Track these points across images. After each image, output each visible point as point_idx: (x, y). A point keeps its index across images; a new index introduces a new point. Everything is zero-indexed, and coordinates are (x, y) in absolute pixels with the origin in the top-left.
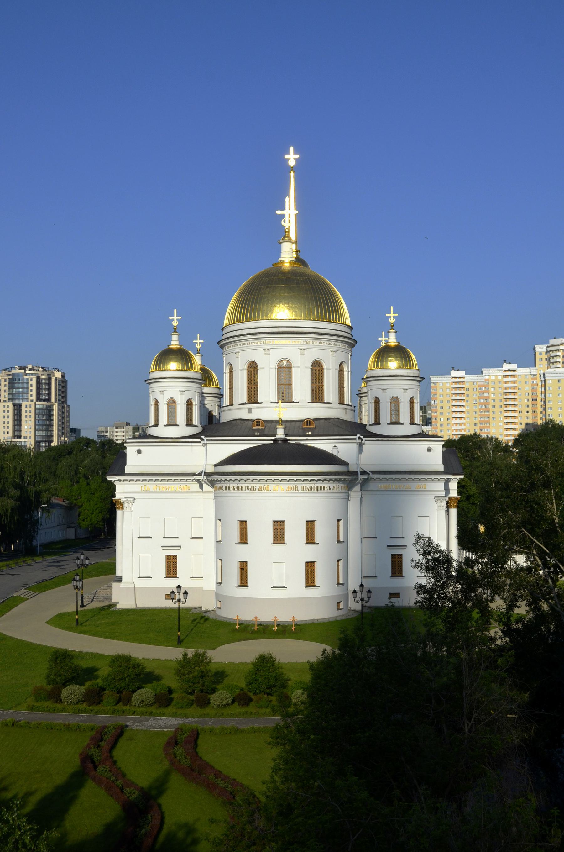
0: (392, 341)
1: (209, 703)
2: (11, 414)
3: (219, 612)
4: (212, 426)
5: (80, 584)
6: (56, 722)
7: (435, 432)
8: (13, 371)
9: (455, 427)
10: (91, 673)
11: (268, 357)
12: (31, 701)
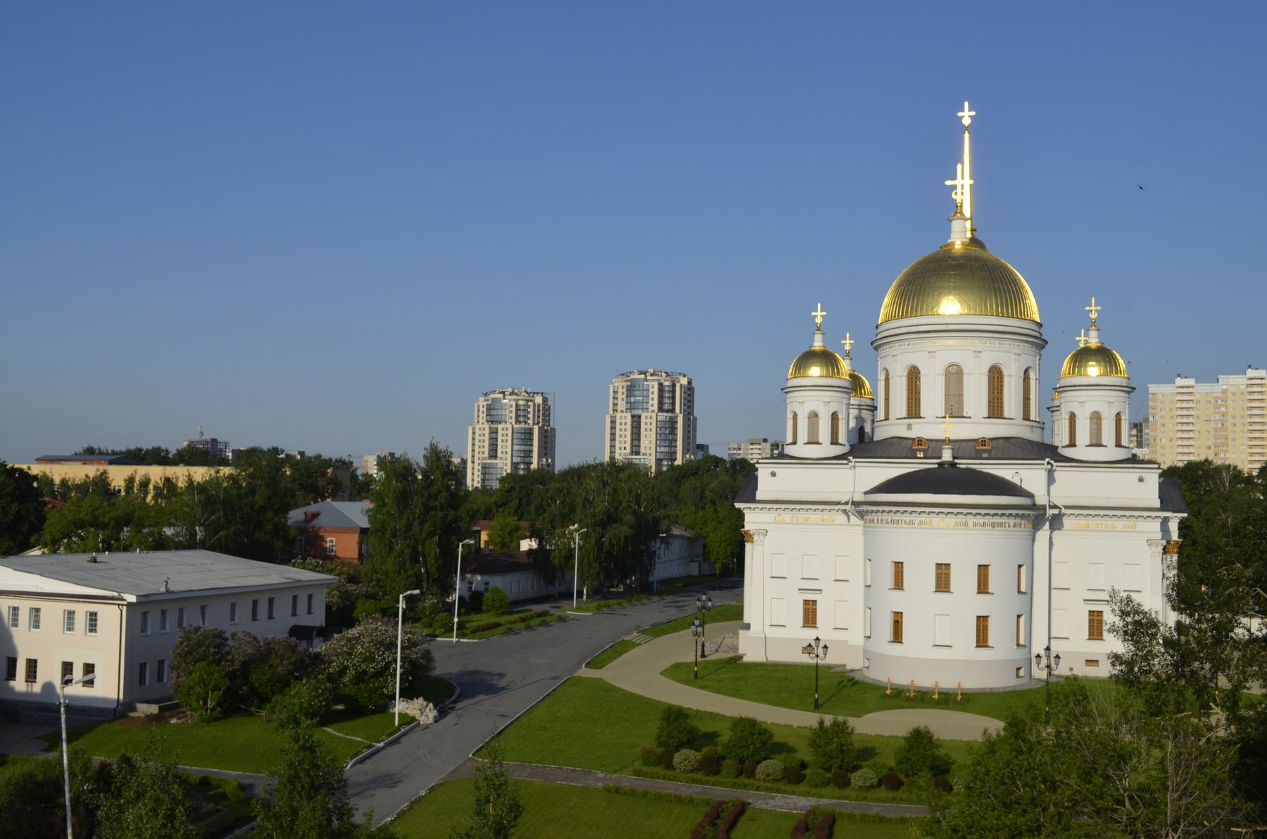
0: (1094, 342)
1: (849, 783)
2: (629, 427)
3: (866, 672)
4: (863, 445)
5: (700, 629)
6: (666, 792)
7: (1152, 457)
8: (632, 377)
9: (1180, 450)
10: (712, 737)
11: (933, 361)
12: (638, 765)
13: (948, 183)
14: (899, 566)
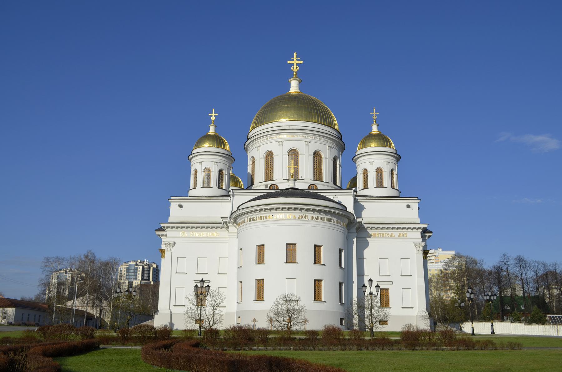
13: (289, 62)
14: (261, 248)
